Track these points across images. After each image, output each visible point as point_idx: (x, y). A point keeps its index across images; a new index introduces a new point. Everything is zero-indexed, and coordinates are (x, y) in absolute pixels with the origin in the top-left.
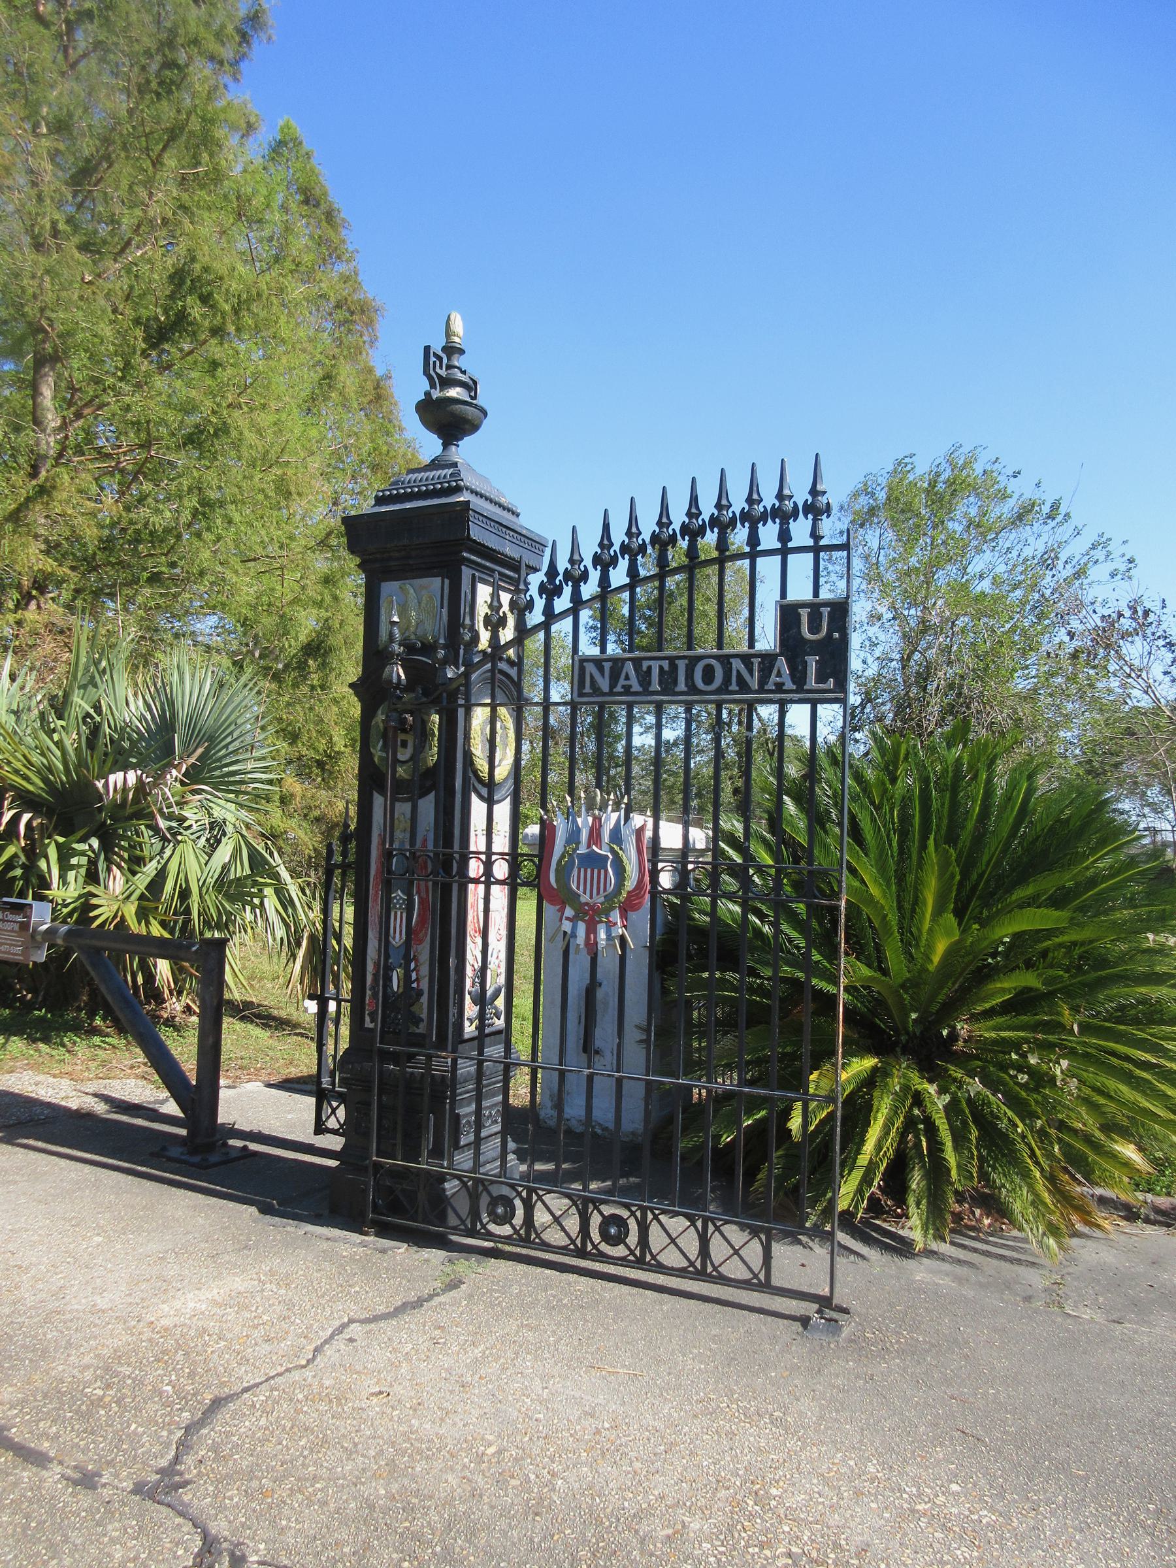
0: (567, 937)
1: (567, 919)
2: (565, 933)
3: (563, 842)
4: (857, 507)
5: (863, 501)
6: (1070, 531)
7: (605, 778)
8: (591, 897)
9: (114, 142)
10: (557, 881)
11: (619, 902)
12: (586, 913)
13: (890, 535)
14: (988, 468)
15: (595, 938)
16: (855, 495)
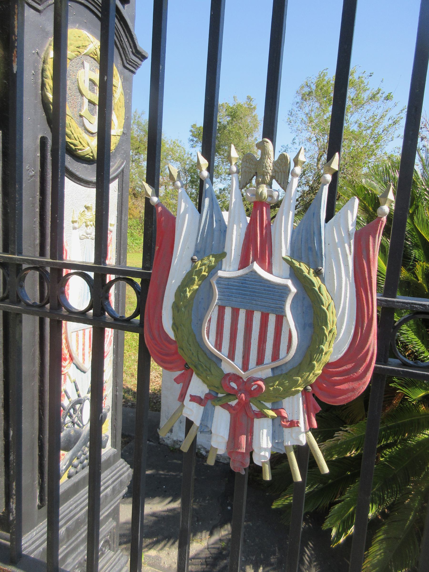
0: (193, 430)
1: (194, 399)
2: (189, 424)
3: (190, 252)
4: (303, 92)
5: (307, 90)
6: (393, 105)
7: (198, 201)
8: (245, 367)
9: (293, 424)
10: (175, 326)
11: (306, 382)
12: (232, 394)
13: (317, 105)
14: (361, 76)
15: (249, 444)
16: (302, 88)
